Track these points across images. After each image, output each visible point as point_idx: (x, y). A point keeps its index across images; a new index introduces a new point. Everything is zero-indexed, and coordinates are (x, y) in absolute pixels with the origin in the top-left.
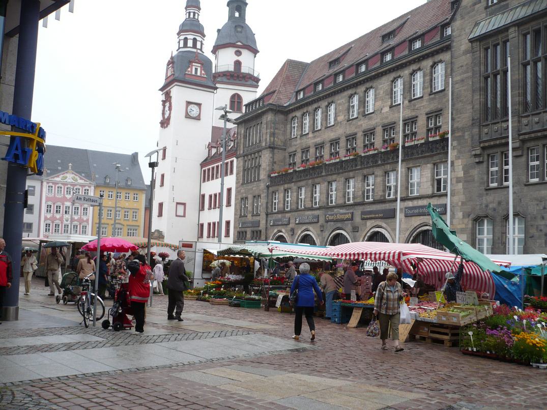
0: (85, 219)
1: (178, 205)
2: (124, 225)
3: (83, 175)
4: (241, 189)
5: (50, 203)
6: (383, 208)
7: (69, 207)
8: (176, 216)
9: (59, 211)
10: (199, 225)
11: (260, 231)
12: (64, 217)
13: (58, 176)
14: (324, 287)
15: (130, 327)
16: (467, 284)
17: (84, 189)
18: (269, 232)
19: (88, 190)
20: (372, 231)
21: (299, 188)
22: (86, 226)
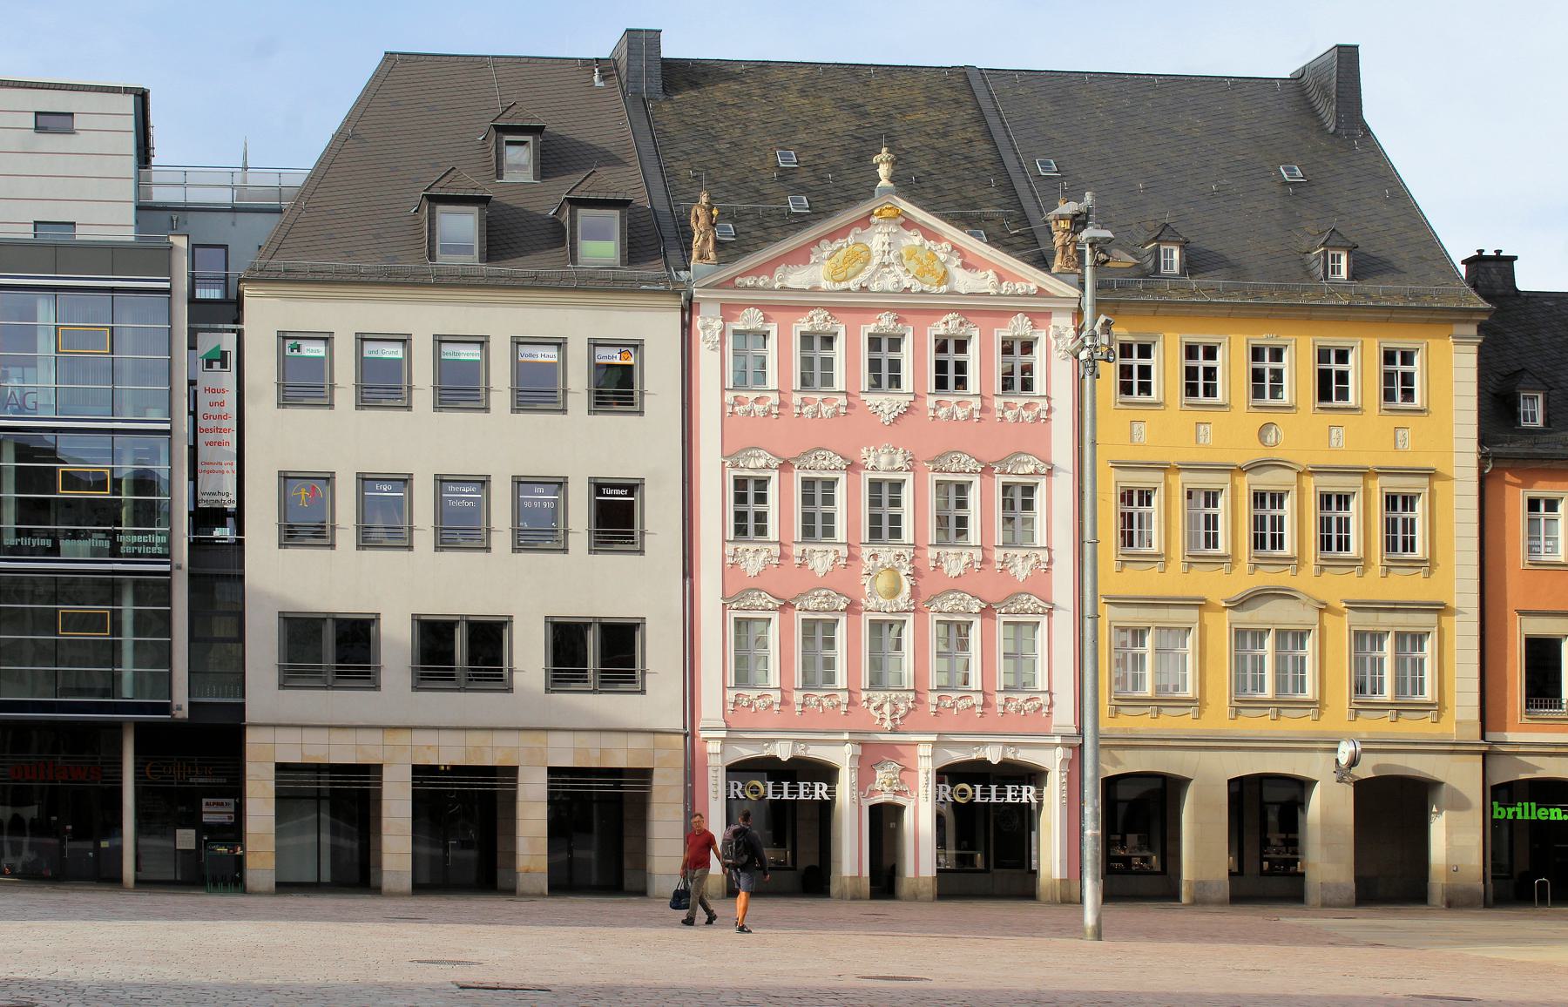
0: (1021, 570)
5: (753, 466)
8: (225, 247)
13: (800, 257)
15: (32, 363)
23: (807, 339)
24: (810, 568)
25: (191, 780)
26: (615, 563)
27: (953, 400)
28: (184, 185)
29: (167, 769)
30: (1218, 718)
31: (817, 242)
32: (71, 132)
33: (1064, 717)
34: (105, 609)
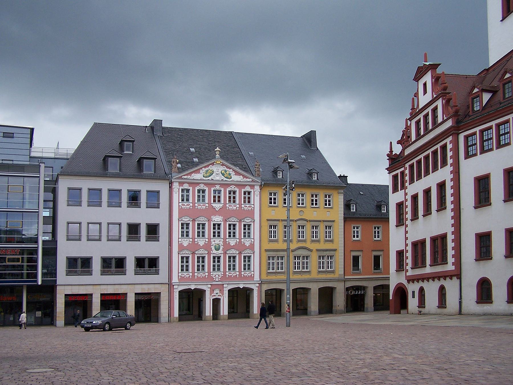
0: (247, 244)
2: (311, 251)
5: (186, 220)
7: (219, 225)
12: (213, 243)
13: (197, 172)
17: (197, 189)
19: (249, 193)
23: (199, 191)
24: (199, 244)
25: (40, 299)
26: (152, 244)
28: (42, 152)
29: (34, 297)
30: (314, 275)
31: (201, 168)
32: (13, 137)
33: (257, 278)
34: (20, 257)
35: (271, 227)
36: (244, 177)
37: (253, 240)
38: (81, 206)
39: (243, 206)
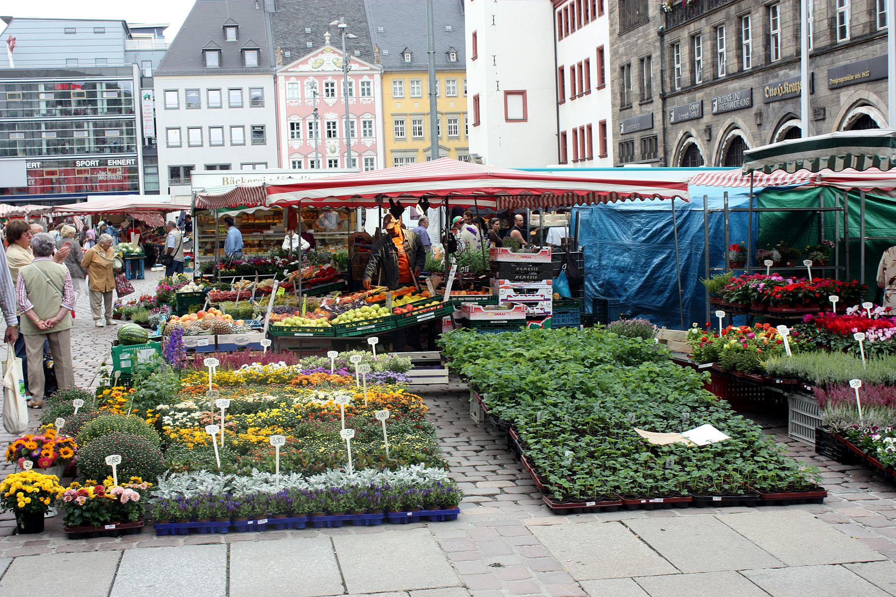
1: (510, 97)
2: (449, 150)
3: (357, 52)
4: (618, 47)
5: (295, 119)
6: (870, 57)
8: (507, 120)
9: (334, 132)
10: (558, 135)
11: (656, 138)
12: (328, 145)
13: (306, 62)
14: (467, 249)
16: (604, 225)
17: (360, 81)
18: (670, 138)
19: (368, 83)
20: (850, 115)
21: (715, 28)
22: (372, 160)
23: (363, 84)
27: (367, 99)
35: (396, 123)
36: (361, 64)
37: (374, 140)
38: (200, 108)
39: (361, 99)
